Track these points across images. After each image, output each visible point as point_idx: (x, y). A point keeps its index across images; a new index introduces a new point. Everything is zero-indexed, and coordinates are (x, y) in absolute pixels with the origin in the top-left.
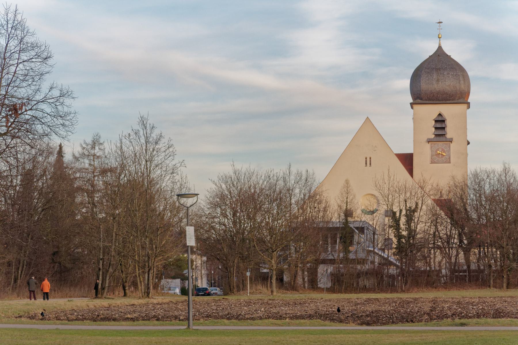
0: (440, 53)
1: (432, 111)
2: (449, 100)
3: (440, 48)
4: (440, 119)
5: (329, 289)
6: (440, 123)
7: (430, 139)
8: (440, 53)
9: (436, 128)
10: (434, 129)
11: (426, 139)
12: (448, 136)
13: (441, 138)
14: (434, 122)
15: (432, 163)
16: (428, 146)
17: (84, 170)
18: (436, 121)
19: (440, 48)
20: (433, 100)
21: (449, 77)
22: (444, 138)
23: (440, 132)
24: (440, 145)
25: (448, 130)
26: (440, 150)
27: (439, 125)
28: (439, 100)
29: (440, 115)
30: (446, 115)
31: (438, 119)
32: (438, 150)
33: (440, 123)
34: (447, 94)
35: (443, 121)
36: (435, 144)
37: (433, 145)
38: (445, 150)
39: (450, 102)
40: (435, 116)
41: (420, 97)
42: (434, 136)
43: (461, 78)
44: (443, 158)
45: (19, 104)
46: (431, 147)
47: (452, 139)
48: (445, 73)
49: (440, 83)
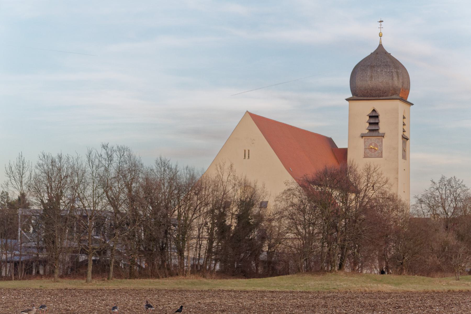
1: (366, 107)
3: (381, 46)
4: (374, 114)
6: (374, 117)
9: (370, 124)
10: (368, 125)
11: (360, 134)
12: (381, 131)
13: (375, 133)
14: (368, 118)
16: (362, 140)
18: (371, 117)
19: (381, 46)
23: (373, 127)
25: (380, 124)
26: (373, 144)
27: (372, 121)
28: (373, 96)
29: (374, 110)
32: (371, 144)
33: (374, 117)
34: (380, 90)
35: (377, 117)
38: (378, 144)
40: (369, 112)
41: (359, 94)
46: (365, 142)
47: (384, 134)
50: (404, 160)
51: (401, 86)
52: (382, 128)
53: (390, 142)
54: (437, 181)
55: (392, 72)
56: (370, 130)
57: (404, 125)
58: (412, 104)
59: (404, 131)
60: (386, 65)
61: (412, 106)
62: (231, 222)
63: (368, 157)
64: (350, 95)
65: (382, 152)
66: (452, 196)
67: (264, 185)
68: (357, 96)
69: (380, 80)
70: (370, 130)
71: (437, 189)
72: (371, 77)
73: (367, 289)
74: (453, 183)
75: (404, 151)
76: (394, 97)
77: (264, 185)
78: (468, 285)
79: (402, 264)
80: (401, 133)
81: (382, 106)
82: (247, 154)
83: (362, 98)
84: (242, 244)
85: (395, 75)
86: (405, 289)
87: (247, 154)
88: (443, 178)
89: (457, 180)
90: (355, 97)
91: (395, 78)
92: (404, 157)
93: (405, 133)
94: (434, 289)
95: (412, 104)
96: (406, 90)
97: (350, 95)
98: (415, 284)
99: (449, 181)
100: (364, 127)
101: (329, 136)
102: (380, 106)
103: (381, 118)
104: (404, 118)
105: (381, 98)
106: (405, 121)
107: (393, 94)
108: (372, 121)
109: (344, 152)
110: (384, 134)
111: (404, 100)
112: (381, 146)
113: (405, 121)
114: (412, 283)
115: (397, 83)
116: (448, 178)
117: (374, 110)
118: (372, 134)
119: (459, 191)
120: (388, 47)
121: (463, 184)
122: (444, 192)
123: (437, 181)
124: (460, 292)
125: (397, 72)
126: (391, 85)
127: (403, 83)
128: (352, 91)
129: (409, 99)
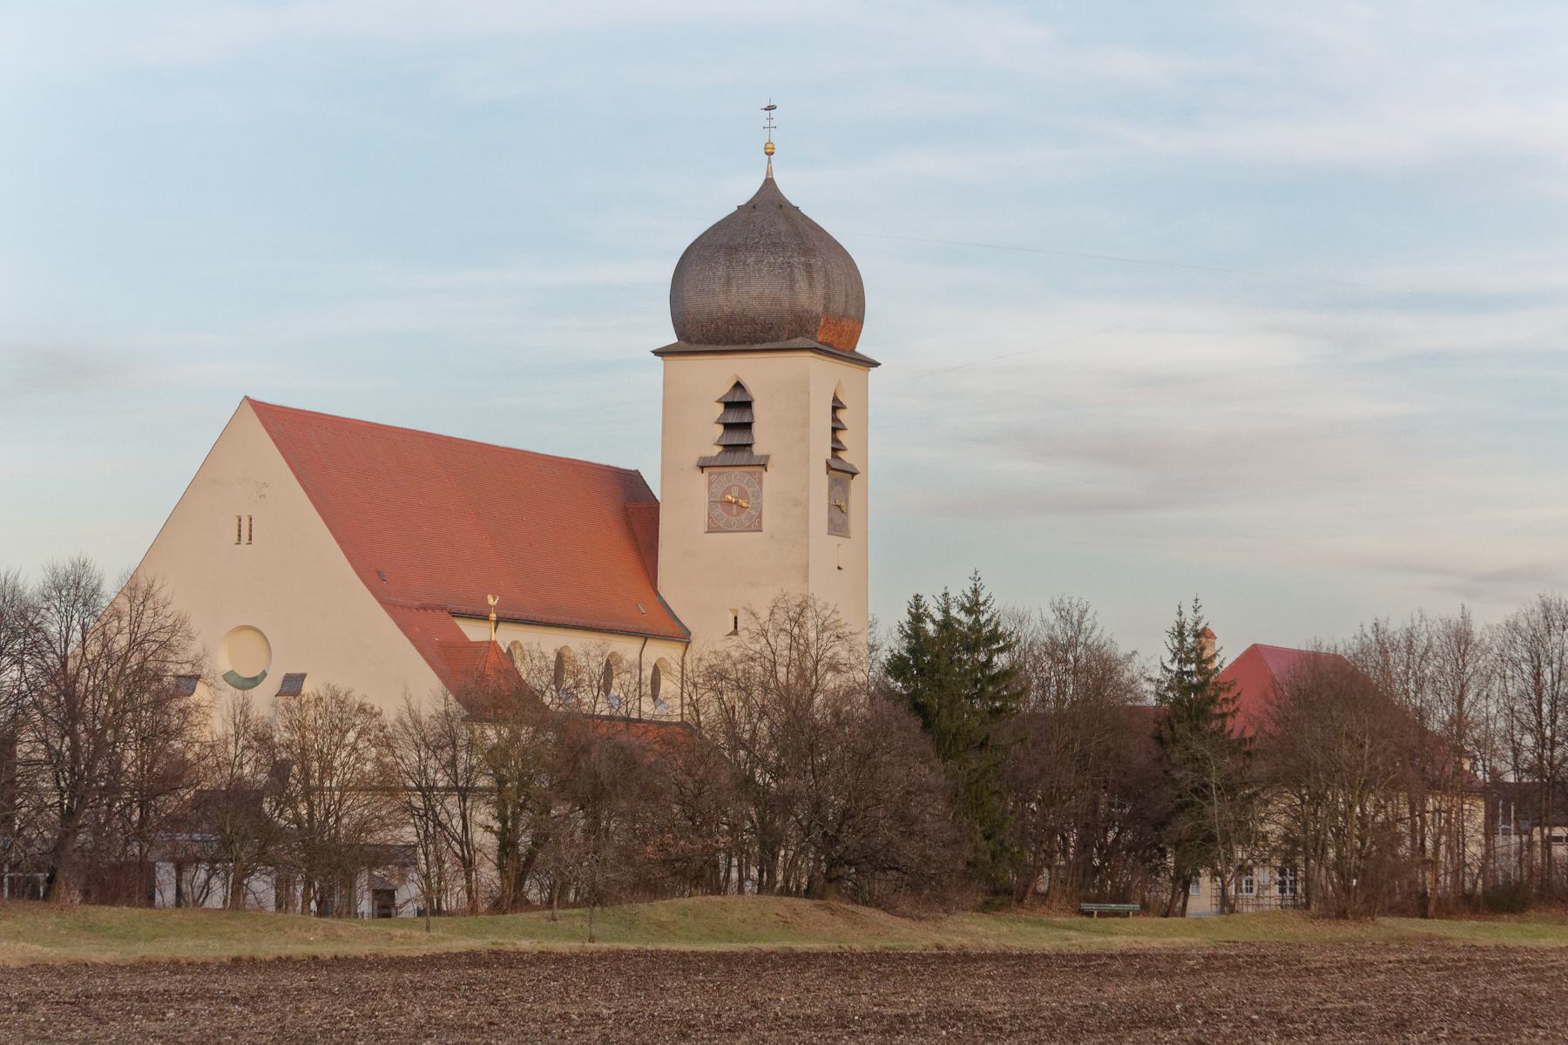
0: (769, 200)
1: (715, 374)
2: (764, 341)
3: (769, 183)
4: (738, 398)
5: (381, 907)
6: (738, 404)
7: (705, 459)
8: (769, 200)
9: (728, 427)
10: (720, 429)
11: (695, 461)
12: (758, 450)
13: (741, 457)
14: (720, 408)
15: (710, 530)
16: (702, 478)
17: (1117, 966)
18: (729, 405)
19: (769, 183)
20: (718, 343)
21: (760, 271)
22: (746, 455)
23: (737, 438)
24: (736, 478)
25: (757, 428)
26: (735, 491)
27: (733, 418)
28: (734, 342)
29: (738, 386)
30: (754, 390)
31: (730, 399)
32: (728, 491)
33: (738, 404)
34: (753, 321)
35: (747, 405)
36: (720, 474)
37: (714, 477)
38: (749, 491)
39: (764, 346)
40: (724, 389)
41: (700, 333)
42: (720, 449)
43: (800, 274)
44: (743, 517)
45: (1522, 694)
46: (710, 484)
47: (768, 457)
48: (750, 260)
49: (734, 289)
51: (820, 309)
52: (763, 439)
55: (791, 266)
58: (876, 364)
60: (774, 245)
61: (873, 370)
64: (670, 338)
65: (760, 516)
68: (688, 340)
69: (755, 289)
72: (728, 282)
82: (245, 532)
85: (800, 274)
87: (245, 532)
91: (802, 285)
95: (876, 364)
97: (670, 338)
100: (708, 437)
102: (759, 372)
104: (837, 406)
105: (757, 346)
110: (768, 457)
112: (758, 495)
115: (808, 297)
117: (738, 386)
120: (792, 190)
126: (786, 305)
127: (828, 299)
129: (862, 348)
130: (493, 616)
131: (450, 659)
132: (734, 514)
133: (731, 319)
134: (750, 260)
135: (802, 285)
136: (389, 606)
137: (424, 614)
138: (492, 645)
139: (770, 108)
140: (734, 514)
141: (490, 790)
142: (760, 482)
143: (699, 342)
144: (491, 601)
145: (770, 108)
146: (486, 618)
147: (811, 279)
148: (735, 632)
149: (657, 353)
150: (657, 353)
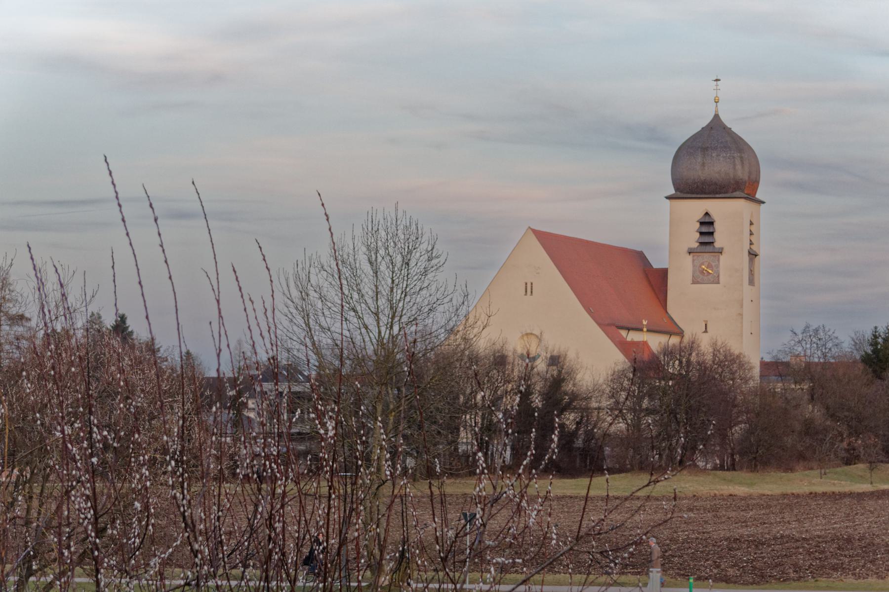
1: (696, 208)
3: (717, 117)
4: (707, 220)
6: (707, 224)
9: (702, 233)
10: (698, 235)
11: (686, 249)
12: (717, 245)
13: (708, 248)
14: (698, 225)
16: (689, 258)
18: (702, 223)
19: (717, 117)
23: (706, 239)
24: (706, 257)
25: (716, 235)
26: (706, 264)
27: (705, 229)
28: (705, 193)
29: (707, 214)
30: (715, 216)
32: (703, 264)
33: (707, 224)
34: (716, 184)
35: (711, 223)
38: (713, 264)
40: (699, 215)
41: (687, 189)
46: (693, 260)
47: (722, 249)
50: (751, 287)
51: (747, 178)
52: (720, 240)
53: (731, 261)
54: (799, 331)
55: (734, 158)
56: (702, 243)
57: (751, 234)
58: (763, 203)
59: (751, 244)
60: (725, 147)
61: (762, 205)
62: (537, 401)
63: (698, 283)
64: (672, 191)
65: (718, 276)
66: (819, 352)
67: (577, 354)
68: (681, 192)
69: (718, 167)
70: (702, 243)
71: (799, 342)
72: (703, 165)
73: (717, 492)
74: (821, 334)
75: (751, 272)
76: (737, 194)
77: (577, 354)
78: (834, 484)
79: (755, 458)
80: (747, 247)
81: (720, 209)
82: (529, 289)
83: (689, 196)
84: (548, 428)
85: (738, 162)
86: (761, 492)
87: (529, 289)
88: (807, 327)
89: (827, 329)
90: (679, 193)
91: (739, 167)
92: (751, 282)
93: (752, 247)
94: (794, 491)
95: (763, 203)
96: (754, 184)
97: (672, 191)
98: (771, 484)
99: (816, 331)
100: (692, 239)
101: (639, 249)
102: (717, 208)
103: (716, 225)
104: (751, 224)
105: (717, 196)
106: (753, 228)
107: (734, 190)
108: (705, 229)
109: (664, 273)
110: (722, 249)
111: (751, 197)
112: (718, 266)
113: (753, 228)
114: (767, 483)
115: (741, 173)
116: (815, 326)
117: (707, 214)
118: (704, 248)
119: (829, 345)
120: (725, 118)
121: (835, 335)
122: (808, 346)
123: (799, 331)
124: (824, 494)
125: (741, 158)
126: (732, 176)
127: (750, 173)
128: (674, 184)
129: (759, 195)
130: (645, 329)
131: (624, 346)
132: (701, 277)
133: (704, 183)
134: (714, 155)
135: (739, 167)
136: (600, 325)
137: (612, 326)
138: (645, 343)
139: (717, 80)
140: (701, 277)
141: (640, 406)
142: (719, 260)
143: (688, 193)
144: (645, 323)
145: (717, 80)
146: (641, 330)
147: (743, 164)
148: (706, 331)
149: (667, 198)
150: (667, 198)
